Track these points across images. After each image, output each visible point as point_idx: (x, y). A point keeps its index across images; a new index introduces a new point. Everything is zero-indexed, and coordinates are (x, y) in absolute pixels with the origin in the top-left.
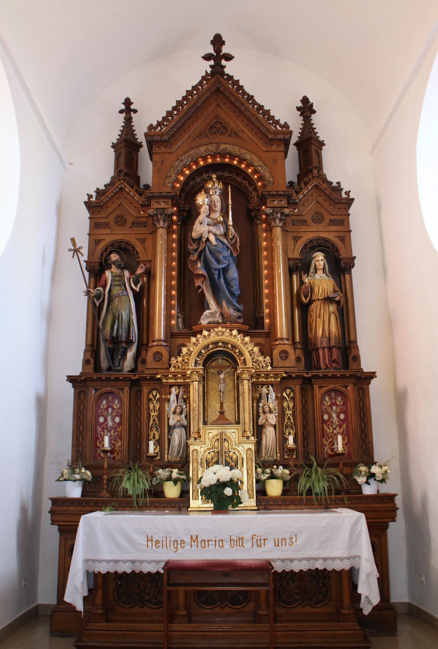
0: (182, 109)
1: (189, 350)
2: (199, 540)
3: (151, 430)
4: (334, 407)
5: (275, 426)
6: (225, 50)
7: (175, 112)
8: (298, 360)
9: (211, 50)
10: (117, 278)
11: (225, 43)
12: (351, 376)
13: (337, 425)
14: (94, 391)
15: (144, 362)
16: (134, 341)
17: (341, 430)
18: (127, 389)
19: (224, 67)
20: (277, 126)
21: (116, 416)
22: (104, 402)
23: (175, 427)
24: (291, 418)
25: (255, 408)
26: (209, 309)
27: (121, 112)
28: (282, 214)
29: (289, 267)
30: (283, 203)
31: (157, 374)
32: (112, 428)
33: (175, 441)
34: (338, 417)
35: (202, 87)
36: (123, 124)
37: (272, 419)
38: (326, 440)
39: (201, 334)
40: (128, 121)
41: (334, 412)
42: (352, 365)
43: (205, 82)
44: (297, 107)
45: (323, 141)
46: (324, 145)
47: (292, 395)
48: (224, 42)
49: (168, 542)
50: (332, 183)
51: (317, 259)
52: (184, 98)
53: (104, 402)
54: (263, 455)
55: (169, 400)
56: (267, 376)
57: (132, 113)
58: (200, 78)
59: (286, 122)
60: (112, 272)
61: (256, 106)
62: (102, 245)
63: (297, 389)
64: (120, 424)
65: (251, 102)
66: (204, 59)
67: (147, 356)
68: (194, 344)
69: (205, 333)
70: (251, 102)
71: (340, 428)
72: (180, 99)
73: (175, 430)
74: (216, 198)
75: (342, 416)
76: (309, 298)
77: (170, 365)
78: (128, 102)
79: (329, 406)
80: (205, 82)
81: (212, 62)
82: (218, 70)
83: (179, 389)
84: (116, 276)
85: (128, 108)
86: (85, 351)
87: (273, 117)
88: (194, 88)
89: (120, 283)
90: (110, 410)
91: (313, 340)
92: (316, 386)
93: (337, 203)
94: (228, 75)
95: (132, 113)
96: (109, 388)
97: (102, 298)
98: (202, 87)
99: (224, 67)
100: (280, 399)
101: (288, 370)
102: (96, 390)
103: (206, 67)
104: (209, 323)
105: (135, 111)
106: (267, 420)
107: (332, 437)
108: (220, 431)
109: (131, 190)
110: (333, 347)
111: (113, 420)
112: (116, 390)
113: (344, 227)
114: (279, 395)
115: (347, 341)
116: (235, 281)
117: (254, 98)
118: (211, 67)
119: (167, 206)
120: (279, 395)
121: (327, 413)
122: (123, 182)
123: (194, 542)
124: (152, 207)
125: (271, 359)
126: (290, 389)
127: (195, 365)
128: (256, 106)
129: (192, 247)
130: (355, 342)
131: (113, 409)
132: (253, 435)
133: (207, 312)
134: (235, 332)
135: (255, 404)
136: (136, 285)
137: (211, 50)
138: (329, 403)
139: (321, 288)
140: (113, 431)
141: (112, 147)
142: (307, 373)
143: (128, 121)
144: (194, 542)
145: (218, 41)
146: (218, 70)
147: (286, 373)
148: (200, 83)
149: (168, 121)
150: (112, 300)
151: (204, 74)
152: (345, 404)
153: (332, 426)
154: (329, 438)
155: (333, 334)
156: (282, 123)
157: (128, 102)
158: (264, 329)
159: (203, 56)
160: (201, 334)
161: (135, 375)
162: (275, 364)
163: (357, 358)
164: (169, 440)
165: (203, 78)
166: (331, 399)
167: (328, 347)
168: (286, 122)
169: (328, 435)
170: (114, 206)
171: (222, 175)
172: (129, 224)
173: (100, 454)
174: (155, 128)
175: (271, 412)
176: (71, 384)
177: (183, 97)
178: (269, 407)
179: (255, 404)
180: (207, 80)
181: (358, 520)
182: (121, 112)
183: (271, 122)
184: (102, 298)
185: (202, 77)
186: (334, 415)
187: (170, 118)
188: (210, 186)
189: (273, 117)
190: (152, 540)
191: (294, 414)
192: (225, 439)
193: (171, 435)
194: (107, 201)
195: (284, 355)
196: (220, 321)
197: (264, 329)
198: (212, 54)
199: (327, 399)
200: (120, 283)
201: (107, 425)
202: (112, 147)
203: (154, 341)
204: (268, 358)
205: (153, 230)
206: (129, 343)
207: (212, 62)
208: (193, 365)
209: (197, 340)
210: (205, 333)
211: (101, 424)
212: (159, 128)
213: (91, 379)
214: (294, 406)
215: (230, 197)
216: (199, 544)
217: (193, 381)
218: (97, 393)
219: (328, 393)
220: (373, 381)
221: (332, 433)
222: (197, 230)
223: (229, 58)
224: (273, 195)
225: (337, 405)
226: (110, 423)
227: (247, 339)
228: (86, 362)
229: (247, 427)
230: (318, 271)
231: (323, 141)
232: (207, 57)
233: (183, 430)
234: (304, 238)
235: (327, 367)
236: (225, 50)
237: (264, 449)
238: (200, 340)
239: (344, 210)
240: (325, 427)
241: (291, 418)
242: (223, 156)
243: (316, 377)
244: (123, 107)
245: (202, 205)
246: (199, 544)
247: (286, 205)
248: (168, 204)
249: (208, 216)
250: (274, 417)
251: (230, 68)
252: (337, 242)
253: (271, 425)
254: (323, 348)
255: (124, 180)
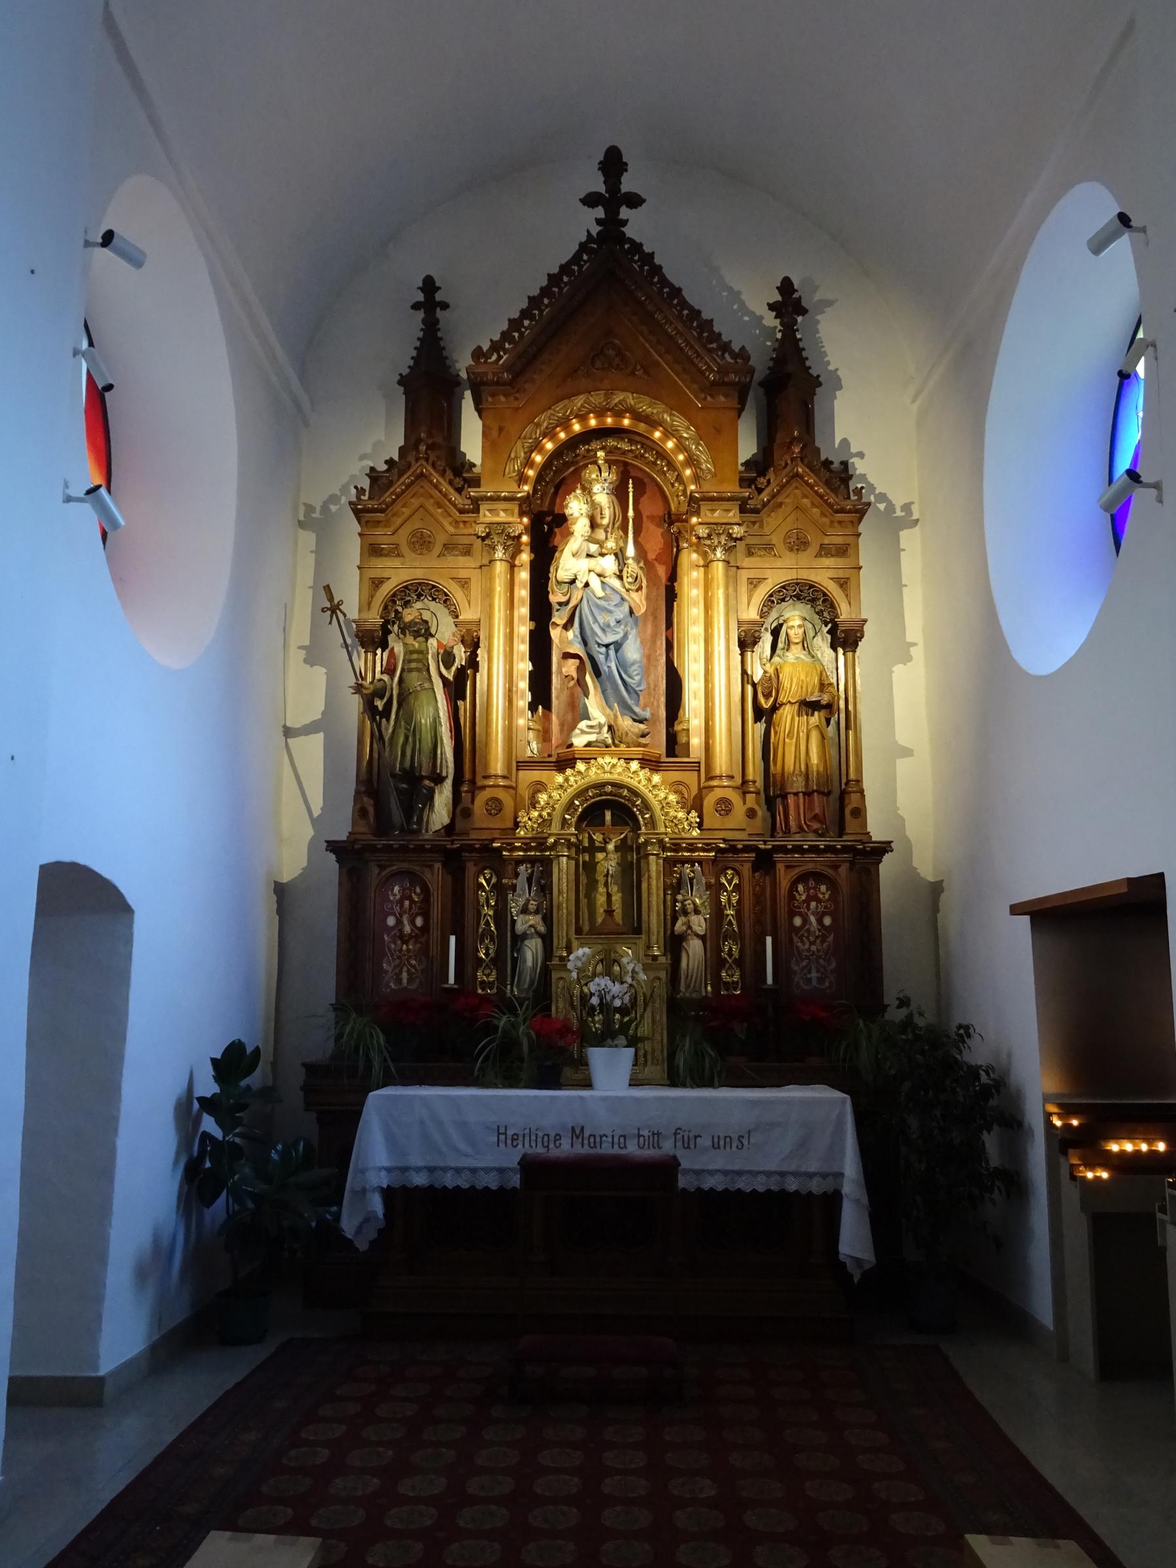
0: (541, 314)
1: (550, 797)
2: (586, 1134)
3: (482, 942)
4: (813, 904)
5: (703, 938)
6: (628, 184)
7: (526, 323)
8: (751, 813)
9: (598, 185)
10: (415, 656)
11: (629, 168)
12: (845, 849)
13: (817, 937)
14: (377, 870)
15: (467, 813)
16: (444, 774)
17: (825, 945)
18: (438, 866)
19: (624, 223)
20: (727, 355)
21: (417, 914)
22: (396, 889)
23: (524, 936)
24: (734, 922)
25: (669, 903)
26: (589, 719)
27: (416, 306)
28: (730, 535)
29: (739, 639)
30: (731, 514)
31: (493, 840)
32: (410, 936)
33: (525, 961)
34: (820, 921)
35: (580, 267)
36: (421, 334)
37: (699, 924)
38: (797, 963)
39: (573, 768)
40: (431, 328)
41: (813, 914)
42: (851, 824)
43: (585, 257)
44: (768, 304)
45: (818, 376)
46: (820, 384)
47: (736, 881)
48: (626, 164)
49: (533, 1138)
50: (832, 463)
51: (791, 624)
52: (545, 291)
53: (396, 889)
54: (682, 989)
55: (514, 888)
56: (692, 848)
57: (438, 310)
58: (575, 247)
59: (743, 347)
60: (405, 644)
61: (685, 312)
62: (386, 589)
63: (746, 869)
64: (425, 928)
65: (675, 302)
66: (584, 204)
67: (473, 802)
68: (561, 786)
69: (581, 766)
70: (675, 302)
71: (823, 942)
72: (536, 292)
73: (527, 942)
74: (602, 497)
75: (827, 921)
76: (772, 699)
77: (516, 825)
78: (429, 286)
79: (804, 901)
80: (585, 257)
81: (600, 212)
82: (612, 227)
83: (533, 867)
84: (412, 652)
85: (430, 300)
86: (357, 792)
87: (720, 334)
88: (565, 269)
89: (420, 665)
90: (407, 903)
91: (778, 778)
92: (780, 867)
93: (837, 512)
94: (631, 241)
95: (438, 310)
96: (405, 865)
97: (387, 695)
98: (580, 267)
99: (624, 223)
100: (716, 889)
101: (729, 835)
102: (382, 867)
103: (589, 220)
104: (589, 744)
105: (445, 306)
106: (690, 927)
107: (807, 957)
108: (605, 946)
109: (441, 480)
110: (814, 791)
111: (412, 922)
112: (417, 868)
113: (847, 560)
114: (713, 881)
115: (844, 780)
116: (635, 667)
117: (684, 293)
118: (599, 222)
119: (510, 519)
120: (713, 881)
121: (800, 914)
122: (424, 463)
123: (577, 1137)
124: (482, 519)
125: (700, 816)
126: (733, 869)
127: (563, 828)
128: (685, 312)
129: (555, 598)
130: (859, 781)
131: (412, 902)
132: (664, 955)
133: (583, 725)
134: (635, 765)
135: (669, 897)
136: (448, 667)
137: (598, 185)
138: (804, 897)
139: (795, 680)
140: (412, 941)
141: (400, 383)
142: (765, 842)
143: (431, 328)
144: (577, 1137)
145: (613, 164)
146: (612, 227)
147: (725, 840)
148: (576, 259)
149: (512, 340)
150: (404, 700)
151: (584, 239)
152: (833, 898)
153: (808, 938)
154: (802, 960)
155: (815, 769)
156: (736, 347)
157: (429, 286)
158: (688, 756)
159: (582, 196)
160: (573, 768)
161: (452, 842)
162: (706, 825)
163: (859, 813)
164: (515, 961)
165: (583, 247)
166: (807, 889)
167: (804, 794)
168: (743, 347)
169: (800, 954)
170: (407, 511)
171: (616, 448)
172: (438, 548)
173: (388, 982)
174: (487, 356)
175: (697, 911)
176: (333, 857)
177: (542, 289)
178: (694, 903)
179: (669, 897)
180: (590, 252)
181: (844, 1101)
182: (416, 306)
183: (714, 345)
184: (387, 695)
185: (581, 244)
186: (813, 919)
187: (516, 335)
188: (594, 476)
189: (720, 334)
190: (505, 1134)
191: (739, 915)
192: (615, 961)
193: (518, 951)
194: (394, 501)
195: (725, 807)
196: (610, 741)
197: (688, 756)
198: (600, 194)
199: (801, 888)
200: (420, 665)
201: (401, 931)
202: (400, 383)
203: (485, 777)
204: (694, 814)
205: (485, 561)
206: (439, 780)
207: (600, 212)
208: (559, 825)
209: (567, 780)
210: (581, 766)
211: (389, 930)
212: (494, 357)
213: (373, 849)
214: (739, 902)
215: (631, 494)
216: (586, 1142)
217: (559, 856)
218: (384, 873)
219: (802, 878)
220: (887, 858)
221: (809, 950)
222: (567, 567)
223: (635, 201)
224: (712, 499)
225: (819, 901)
226: (407, 929)
227: (656, 778)
228: (361, 812)
229: (654, 938)
230: (793, 647)
231: (818, 376)
232: (591, 200)
233: (539, 941)
234: (770, 581)
235: (801, 830)
236: (628, 184)
237: (683, 977)
238: (572, 779)
239: (850, 525)
240: (795, 939)
241: (734, 922)
242: (619, 415)
243: (783, 849)
244: (420, 297)
245: (577, 519)
246: (586, 1142)
247: (737, 520)
248: (513, 515)
249: (590, 539)
250: (703, 921)
251: (637, 225)
252: (833, 589)
253: (697, 935)
254: (796, 794)
255: (427, 460)
